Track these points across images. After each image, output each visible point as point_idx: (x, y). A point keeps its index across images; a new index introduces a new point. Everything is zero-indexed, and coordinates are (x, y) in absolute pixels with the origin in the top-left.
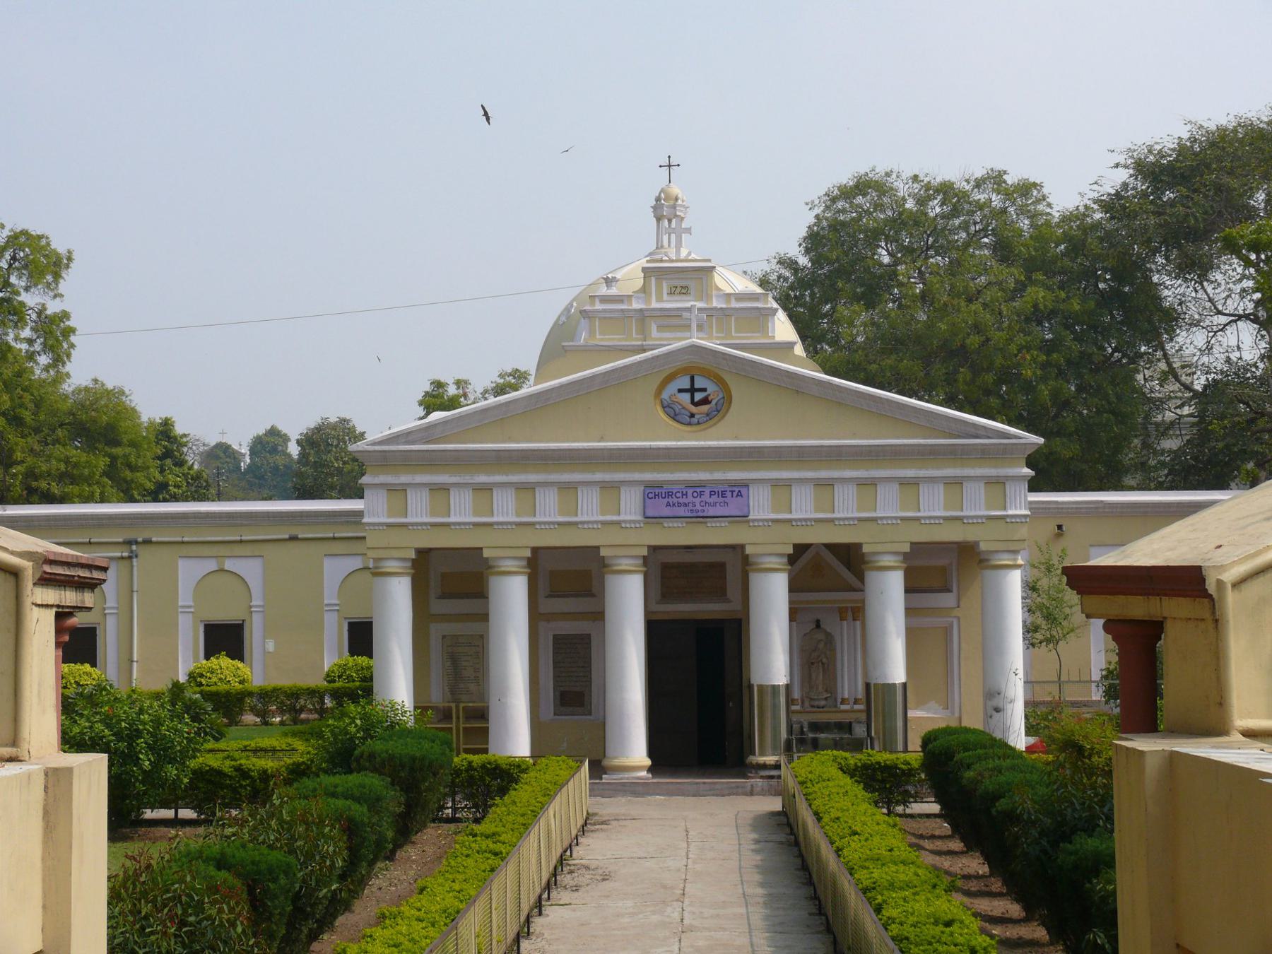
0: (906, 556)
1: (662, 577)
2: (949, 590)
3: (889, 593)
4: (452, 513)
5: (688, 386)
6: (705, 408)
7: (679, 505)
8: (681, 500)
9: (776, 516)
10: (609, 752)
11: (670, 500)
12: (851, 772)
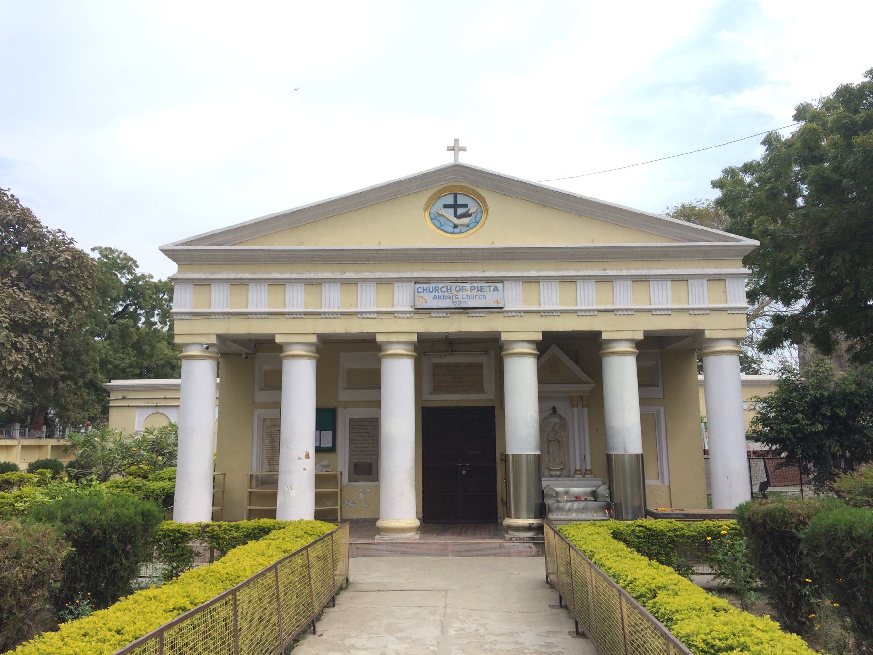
0: (638, 344)
2: (657, 385)
3: (622, 377)
4: (250, 304)
5: (451, 202)
6: (466, 220)
7: (444, 298)
9: (523, 313)
10: (383, 514)
11: (437, 293)
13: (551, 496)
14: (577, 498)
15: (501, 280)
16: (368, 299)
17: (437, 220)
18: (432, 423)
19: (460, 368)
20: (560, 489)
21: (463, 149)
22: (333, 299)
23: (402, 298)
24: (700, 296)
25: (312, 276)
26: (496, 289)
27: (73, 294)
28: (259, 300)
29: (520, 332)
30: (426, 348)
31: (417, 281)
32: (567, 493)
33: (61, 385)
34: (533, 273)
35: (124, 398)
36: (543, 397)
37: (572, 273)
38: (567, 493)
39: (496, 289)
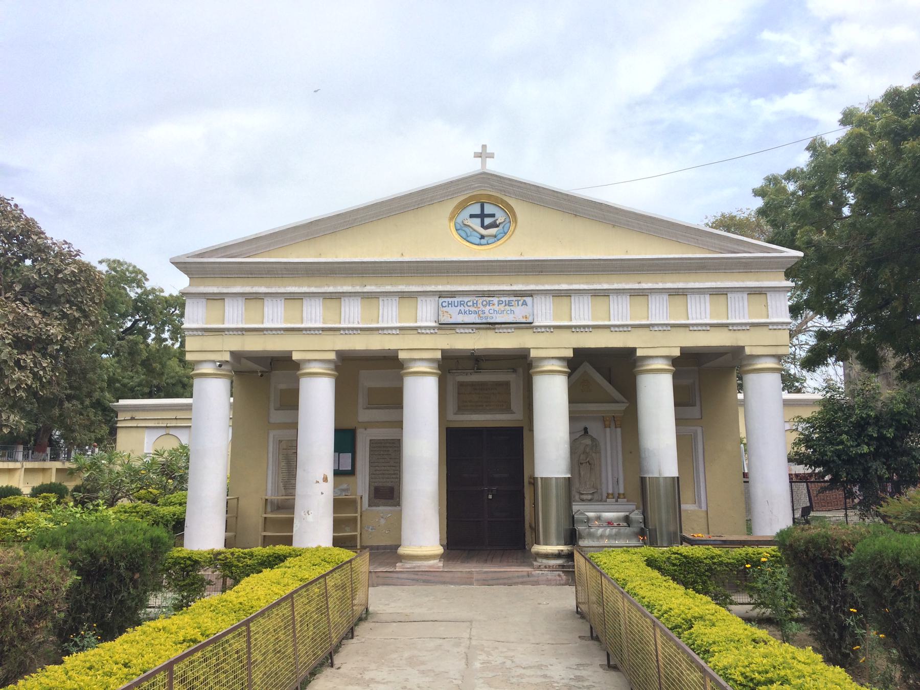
0: (675, 361)
1: (459, 394)
2: (694, 405)
3: (657, 394)
5: (478, 212)
6: (493, 231)
7: (470, 312)
8: (472, 309)
9: (554, 328)
11: (462, 308)
12: (651, 563)
13: (582, 522)
14: (610, 523)
15: (530, 294)
16: (390, 314)
17: (463, 231)
18: (457, 444)
19: (487, 386)
20: (591, 515)
21: (491, 156)
22: (353, 314)
23: (426, 314)
24: (740, 311)
25: (331, 289)
26: (525, 303)
27: (80, 309)
28: (274, 315)
29: (550, 350)
30: (451, 365)
31: (441, 295)
32: (599, 518)
33: (67, 405)
34: (564, 287)
35: (133, 419)
36: (573, 418)
37: (606, 286)
38: (599, 518)
39: (525, 303)
